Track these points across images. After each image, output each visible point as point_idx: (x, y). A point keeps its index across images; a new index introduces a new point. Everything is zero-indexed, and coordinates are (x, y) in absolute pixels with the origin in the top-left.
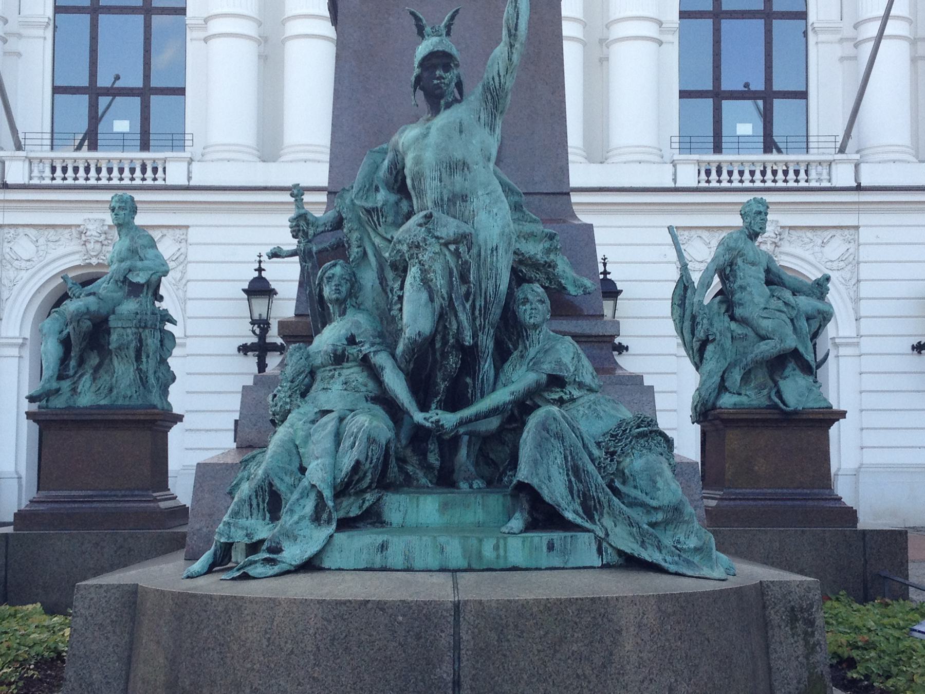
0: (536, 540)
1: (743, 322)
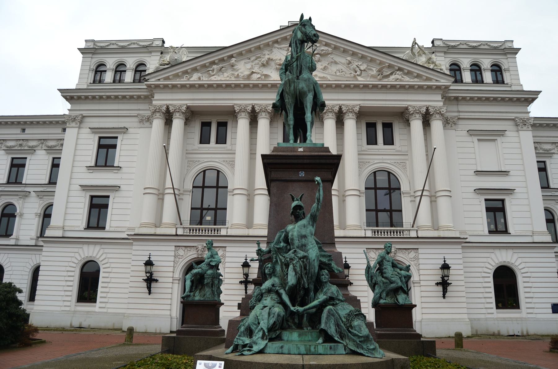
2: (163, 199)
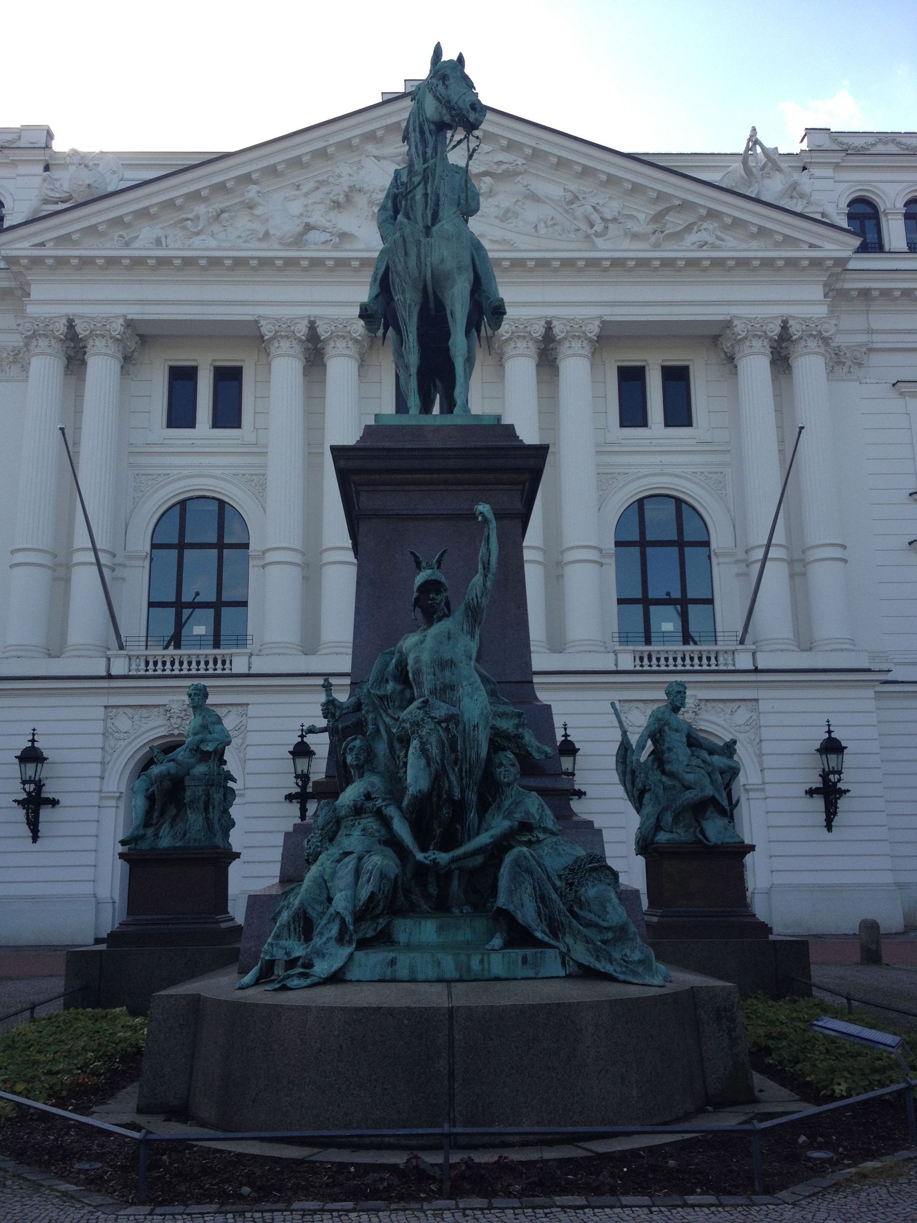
0: (513, 955)
1: (672, 775)
2: (67, 580)
